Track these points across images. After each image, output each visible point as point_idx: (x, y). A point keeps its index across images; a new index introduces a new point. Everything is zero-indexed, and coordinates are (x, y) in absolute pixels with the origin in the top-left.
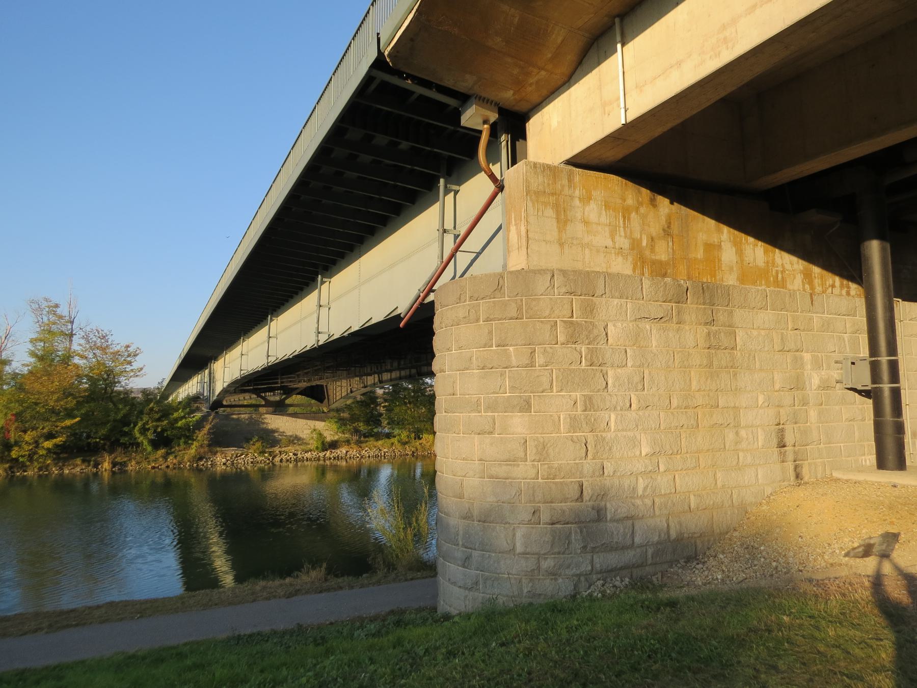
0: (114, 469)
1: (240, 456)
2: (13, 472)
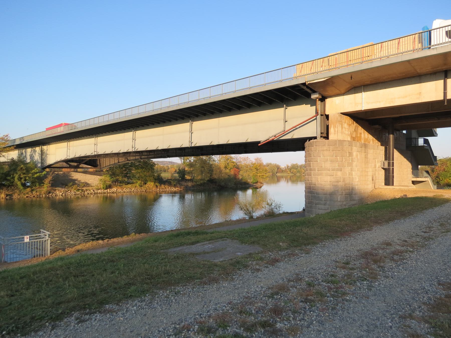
0: (7, 198)
1: (67, 192)
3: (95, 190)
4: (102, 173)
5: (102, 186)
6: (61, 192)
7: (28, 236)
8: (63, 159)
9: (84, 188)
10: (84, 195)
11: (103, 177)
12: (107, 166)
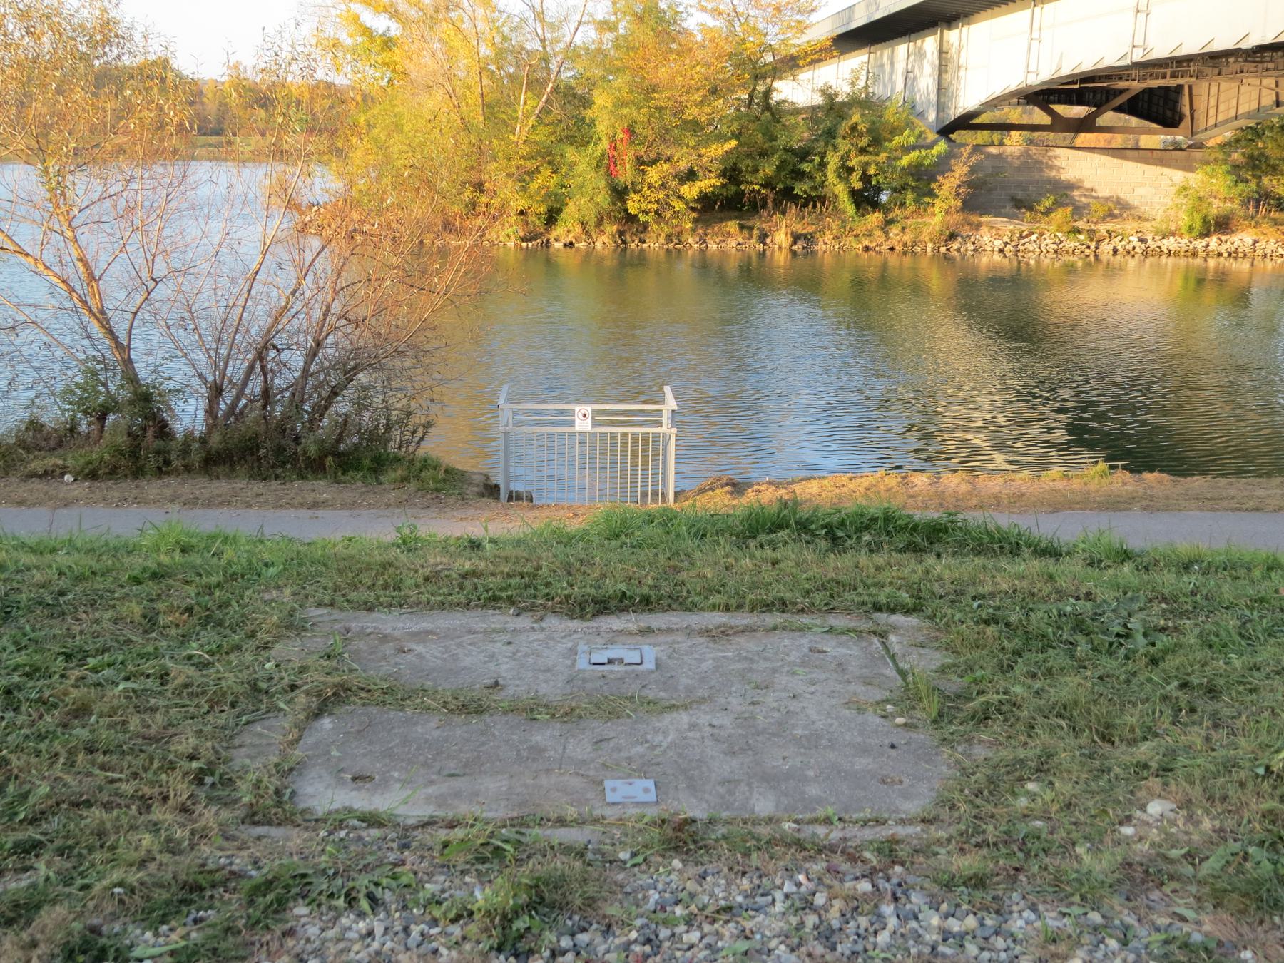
0: (795, 248)
1: (1027, 236)
2: (624, 242)
3: (1149, 237)
4: (1198, 154)
5: (1184, 220)
6: (999, 237)
7: (589, 409)
8: (1013, 87)
9: (1102, 228)
10: (1096, 256)
11: (1195, 179)
12: (1226, 122)
